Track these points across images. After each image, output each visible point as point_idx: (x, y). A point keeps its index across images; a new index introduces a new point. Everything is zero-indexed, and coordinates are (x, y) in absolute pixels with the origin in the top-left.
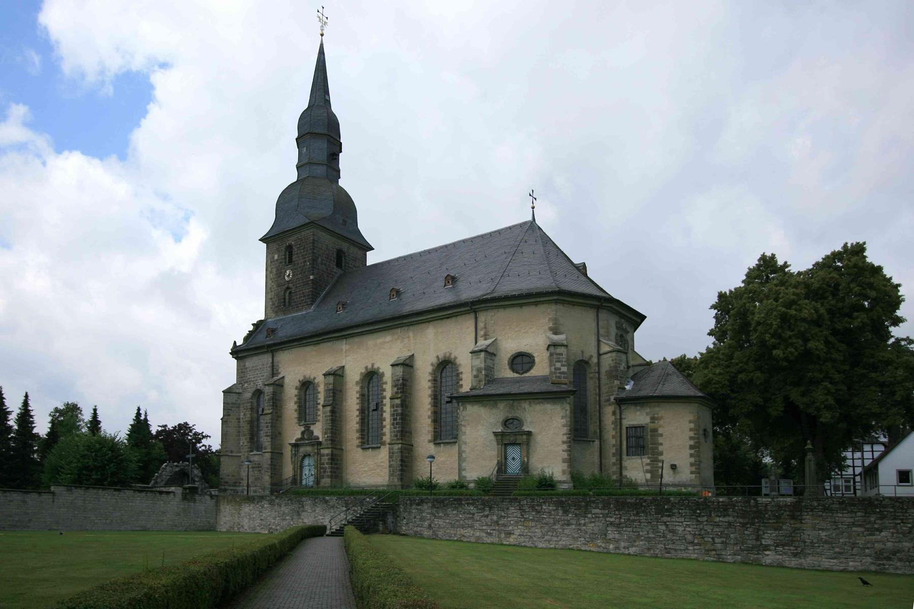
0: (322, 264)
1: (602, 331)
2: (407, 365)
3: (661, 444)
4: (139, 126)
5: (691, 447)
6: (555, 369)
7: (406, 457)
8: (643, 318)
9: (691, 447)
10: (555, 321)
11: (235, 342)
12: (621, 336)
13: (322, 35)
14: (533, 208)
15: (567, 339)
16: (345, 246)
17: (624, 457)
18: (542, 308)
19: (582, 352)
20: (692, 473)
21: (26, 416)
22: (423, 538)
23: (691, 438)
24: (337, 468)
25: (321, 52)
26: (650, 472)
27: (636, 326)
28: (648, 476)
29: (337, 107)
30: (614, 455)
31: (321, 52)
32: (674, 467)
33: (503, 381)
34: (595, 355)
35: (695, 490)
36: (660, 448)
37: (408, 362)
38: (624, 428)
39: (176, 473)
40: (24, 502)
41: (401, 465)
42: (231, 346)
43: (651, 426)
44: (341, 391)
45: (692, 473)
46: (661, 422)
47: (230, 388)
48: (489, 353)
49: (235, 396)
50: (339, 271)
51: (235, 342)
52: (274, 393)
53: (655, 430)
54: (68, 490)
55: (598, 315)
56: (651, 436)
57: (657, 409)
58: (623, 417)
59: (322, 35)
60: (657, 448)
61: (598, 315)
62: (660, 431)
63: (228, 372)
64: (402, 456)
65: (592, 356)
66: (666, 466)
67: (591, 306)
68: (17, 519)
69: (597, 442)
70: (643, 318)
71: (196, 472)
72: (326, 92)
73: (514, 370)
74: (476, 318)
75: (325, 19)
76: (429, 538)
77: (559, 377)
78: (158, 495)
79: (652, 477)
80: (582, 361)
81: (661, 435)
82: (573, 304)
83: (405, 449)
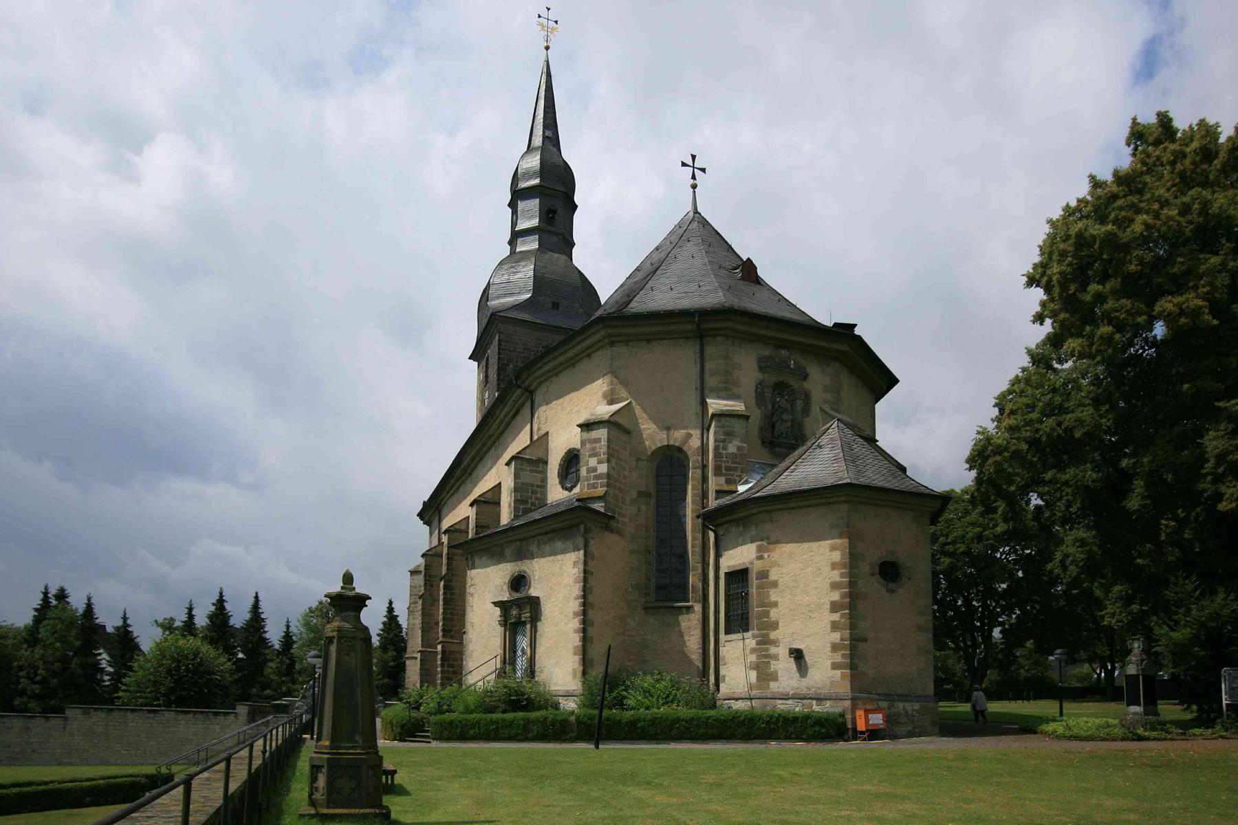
1: (711, 382)
3: (775, 604)
4: (1001, 403)
5: (834, 607)
8: (892, 381)
9: (834, 607)
13: (547, 48)
14: (694, 187)
15: (598, 403)
17: (723, 637)
20: (835, 666)
22: (856, 735)
23: (834, 586)
27: (879, 394)
28: (753, 675)
29: (570, 153)
32: (798, 655)
35: (827, 708)
36: (774, 613)
38: (722, 576)
40: (27, 729)
43: (758, 566)
45: (835, 666)
53: (763, 575)
54: (84, 713)
56: (758, 587)
59: (547, 48)
60: (767, 614)
66: (782, 651)
67: (685, 336)
68: (17, 750)
69: (698, 608)
70: (892, 381)
73: (564, 488)
75: (552, 24)
76: (874, 734)
78: (211, 716)
79: (758, 678)
81: (775, 584)
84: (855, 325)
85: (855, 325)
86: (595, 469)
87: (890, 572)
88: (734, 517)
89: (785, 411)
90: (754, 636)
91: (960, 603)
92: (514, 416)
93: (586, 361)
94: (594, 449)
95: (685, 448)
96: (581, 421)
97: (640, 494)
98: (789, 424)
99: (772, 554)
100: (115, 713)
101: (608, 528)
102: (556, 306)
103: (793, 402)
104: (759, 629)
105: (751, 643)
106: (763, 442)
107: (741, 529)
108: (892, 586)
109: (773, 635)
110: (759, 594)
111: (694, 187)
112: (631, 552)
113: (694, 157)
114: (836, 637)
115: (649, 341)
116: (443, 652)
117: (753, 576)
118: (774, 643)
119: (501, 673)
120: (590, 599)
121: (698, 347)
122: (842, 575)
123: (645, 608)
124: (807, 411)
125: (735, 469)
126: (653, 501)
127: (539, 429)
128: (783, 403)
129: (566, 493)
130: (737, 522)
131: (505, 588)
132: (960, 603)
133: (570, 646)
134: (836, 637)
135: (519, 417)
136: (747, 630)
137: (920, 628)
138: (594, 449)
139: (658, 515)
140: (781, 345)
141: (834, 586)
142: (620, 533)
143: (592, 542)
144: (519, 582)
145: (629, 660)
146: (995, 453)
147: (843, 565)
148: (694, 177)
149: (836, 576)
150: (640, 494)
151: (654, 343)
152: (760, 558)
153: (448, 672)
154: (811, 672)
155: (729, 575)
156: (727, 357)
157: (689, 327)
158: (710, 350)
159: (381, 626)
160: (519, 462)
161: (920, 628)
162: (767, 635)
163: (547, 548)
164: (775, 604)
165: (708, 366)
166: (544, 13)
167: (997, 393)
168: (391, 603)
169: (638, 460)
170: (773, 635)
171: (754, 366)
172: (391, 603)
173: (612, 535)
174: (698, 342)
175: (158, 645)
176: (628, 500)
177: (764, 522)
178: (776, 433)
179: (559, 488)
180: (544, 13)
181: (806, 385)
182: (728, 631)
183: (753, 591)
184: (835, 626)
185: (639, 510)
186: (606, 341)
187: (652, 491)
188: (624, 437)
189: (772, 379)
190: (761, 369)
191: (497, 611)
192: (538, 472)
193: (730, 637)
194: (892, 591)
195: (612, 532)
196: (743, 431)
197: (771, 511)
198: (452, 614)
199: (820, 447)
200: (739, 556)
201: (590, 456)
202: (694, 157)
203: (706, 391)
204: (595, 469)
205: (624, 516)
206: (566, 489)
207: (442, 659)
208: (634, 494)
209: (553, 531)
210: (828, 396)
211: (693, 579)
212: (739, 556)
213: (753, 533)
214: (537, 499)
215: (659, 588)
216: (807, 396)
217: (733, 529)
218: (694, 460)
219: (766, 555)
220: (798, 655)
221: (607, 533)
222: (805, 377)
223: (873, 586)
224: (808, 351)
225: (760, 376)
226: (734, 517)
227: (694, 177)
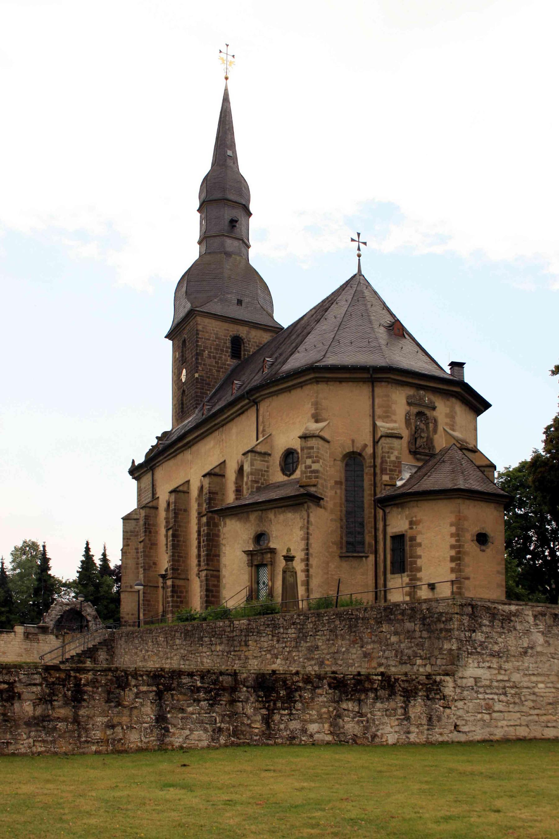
0: (210, 357)
1: (378, 411)
2: (216, 475)
3: (420, 557)
5: (453, 559)
6: (306, 467)
7: (214, 586)
9: (453, 559)
10: (316, 405)
11: (133, 462)
12: (420, 414)
13: (227, 78)
14: (359, 256)
16: (242, 331)
17: (389, 576)
18: (297, 394)
19: (353, 441)
21: (105, 559)
24: (181, 602)
25: (226, 100)
26: (409, 594)
31: (226, 100)
33: (278, 486)
34: (370, 444)
36: (419, 562)
37: (217, 470)
39: (65, 612)
41: (207, 596)
42: (129, 465)
44: (185, 510)
46: (420, 527)
47: (129, 514)
48: (260, 453)
49: (133, 523)
50: (235, 362)
51: (133, 462)
52: (147, 517)
53: (413, 539)
55: (373, 391)
57: (415, 510)
58: (387, 523)
59: (227, 78)
60: (415, 562)
61: (373, 391)
62: (419, 540)
63: (126, 496)
64: (207, 585)
65: (366, 446)
69: (372, 558)
71: (89, 610)
72: (232, 146)
73: (284, 474)
74: (257, 410)
75: (230, 58)
77: (310, 478)
80: (353, 452)
81: (420, 545)
82: (341, 381)
83: (212, 576)
86: (310, 467)
87: (482, 539)
88: (397, 502)
89: (423, 431)
90: (408, 576)
91: (547, 554)
92: (239, 415)
93: (299, 390)
95: (364, 454)
96: (300, 434)
97: (336, 483)
98: (425, 440)
99: (418, 527)
101: (319, 506)
102: (240, 302)
103: (427, 425)
104: (411, 572)
105: (406, 580)
106: (410, 452)
107: (400, 510)
108: (483, 547)
109: (419, 575)
110: (411, 550)
111: (359, 256)
112: (331, 520)
113: (359, 234)
115: (341, 382)
116: (173, 586)
117: (407, 539)
118: (420, 579)
119: (250, 598)
120: (311, 551)
121: (371, 390)
123: (341, 557)
124: (435, 431)
125: (395, 470)
126: (344, 487)
127: (264, 430)
128: (422, 426)
129: (286, 478)
130: (397, 505)
131: (251, 541)
132: (547, 554)
135: (244, 417)
136: (404, 572)
137: (498, 572)
138: (309, 453)
139: (346, 497)
140: (419, 387)
142: (325, 508)
143: (311, 515)
144: (259, 537)
145: (331, 590)
146: (540, 466)
148: (359, 249)
150: (336, 483)
151: (344, 384)
152: (411, 528)
153: (177, 602)
154: (403, 435)
155: (394, 538)
157: (366, 376)
158: (378, 391)
159: (80, 564)
160: (253, 454)
161: (498, 572)
162: (415, 575)
164: (420, 557)
165: (377, 401)
166: (224, 49)
167: (545, 426)
168: (87, 544)
169: (335, 460)
170: (419, 575)
171: (404, 401)
172: (87, 544)
173: (321, 509)
176: (329, 485)
177: (413, 507)
178: (417, 445)
179: (280, 474)
180: (224, 49)
181: (435, 413)
182: (393, 573)
183: (407, 548)
185: (336, 493)
186: (314, 380)
187: (343, 481)
188: (326, 445)
189: (414, 410)
190: (409, 404)
191: (245, 558)
192: (264, 461)
193: (393, 576)
194: (483, 551)
195: (321, 508)
196: (399, 447)
197: (417, 501)
198: (179, 556)
199: (444, 462)
200: (398, 523)
201: (307, 458)
202: (359, 234)
203: (376, 417)
204: (310, 467)
205: (327, 497)
206: (286, 475)
207: (173, 591)
208: (332, 482)
210: (448, 420)
211: (368, 539)
212: (398, 523)
213: (407, 513)
214: (265, 480)
215: (348, 543)
216: (436, 421)
217: (395, 509)
218: (369, 461)
219: (414, 527)
221: (318, 508)
222: (434, 408)
223: (471, 547)
224: (435, 391)
225: (408, 408)
226: (397, 502)
227: (359, 249)
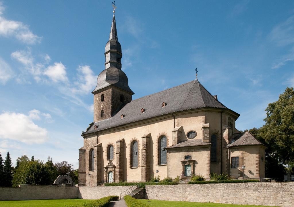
3: (245, 163)
5: (256, 164)
30: (226, 168)
68: (7, 197)
69: (220, 163)
81: (245, 160)
84: (134, 94)
85: (134, 94)
94: (206, 132)
100: (33, 186)
114: (257, 169)
122: (258, 159)
127: (178, 125)
133: (206, 170)
134: (257, 169)
138: (206, 132)
141: (257, 161)
147: (258, 157)
149: (257, 159)
151: (213, 113)
156: (225, 117)
163: (199, 150)
165: (222, 118)
174: (221, 113)
175: (69, 168)
184: (257, 167)
201: (205, 134)
204: (206, 136)
209: (202, 148)
220: (250, 172)
